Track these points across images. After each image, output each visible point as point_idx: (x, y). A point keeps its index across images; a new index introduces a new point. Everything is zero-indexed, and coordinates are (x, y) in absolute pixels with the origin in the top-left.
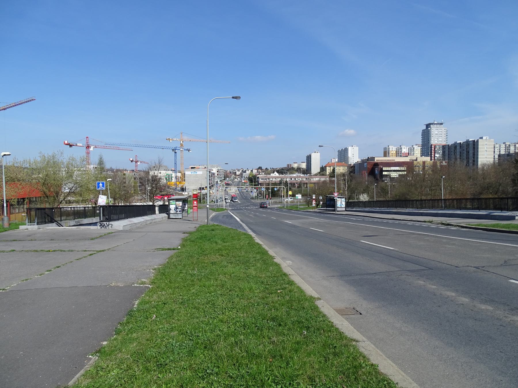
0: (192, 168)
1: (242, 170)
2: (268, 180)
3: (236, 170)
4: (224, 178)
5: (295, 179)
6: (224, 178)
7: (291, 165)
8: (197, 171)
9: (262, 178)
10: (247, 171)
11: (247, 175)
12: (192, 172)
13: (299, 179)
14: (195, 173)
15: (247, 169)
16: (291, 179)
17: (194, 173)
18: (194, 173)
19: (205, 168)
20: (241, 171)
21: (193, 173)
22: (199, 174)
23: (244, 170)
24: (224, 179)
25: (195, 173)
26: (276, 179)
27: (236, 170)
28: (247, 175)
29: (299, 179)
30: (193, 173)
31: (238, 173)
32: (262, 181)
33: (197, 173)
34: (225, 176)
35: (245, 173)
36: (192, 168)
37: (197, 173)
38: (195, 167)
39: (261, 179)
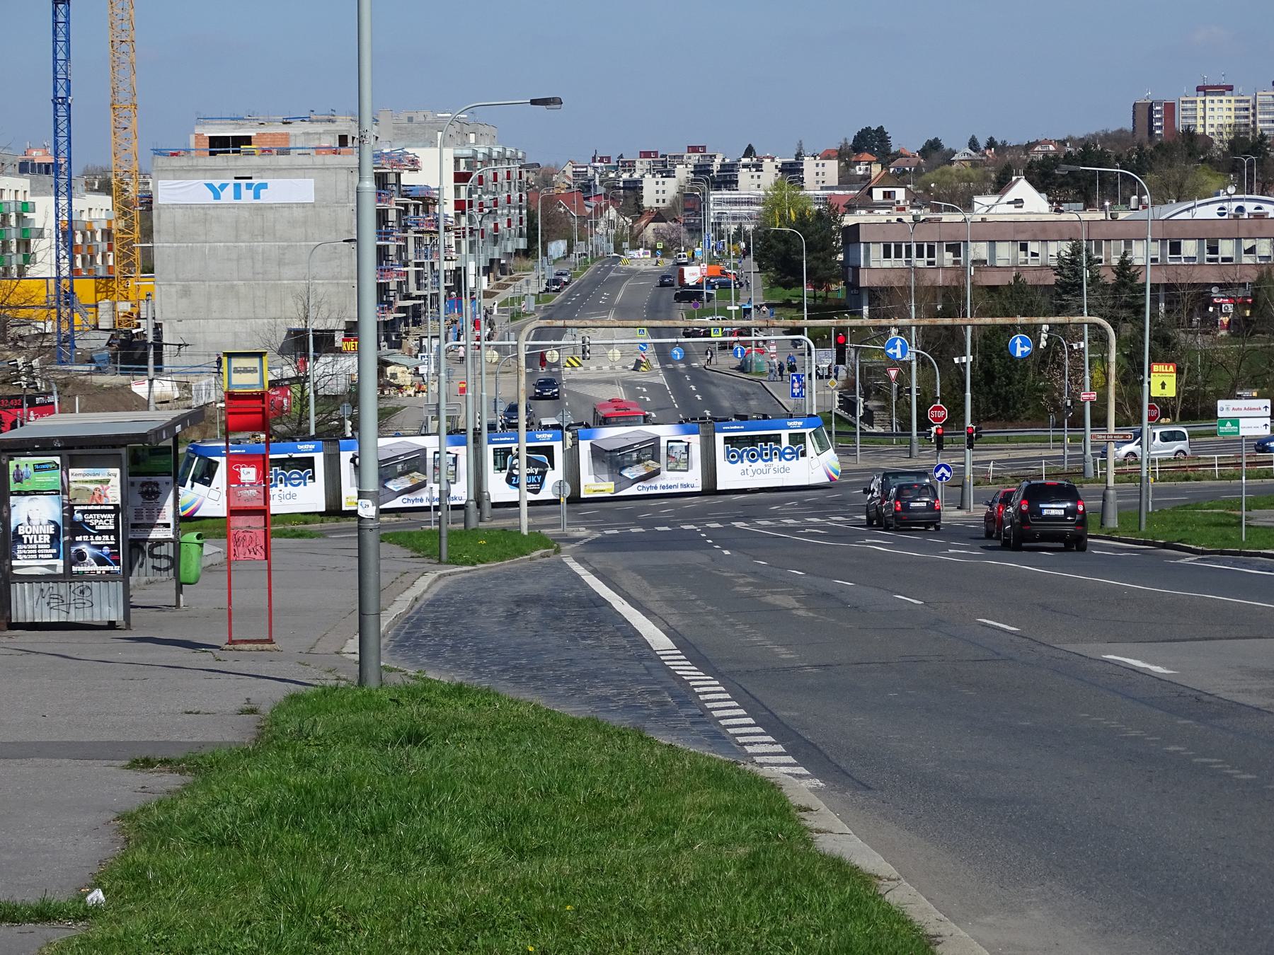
0: (219, 145)
1: (695, 158)
2: (949, 256)
3: (641, 165)
4: (522, 244)
5: (1214, 250)
6: (522, 244)
7: (1170, 108)
8: (262, 170)
9: (893, 238)
10: (744, 176)
11: (744, 210)
12: (217, 183)
13: (1247, 244)
14: (248, 196)
15: (749, 152)
16: (1176, 248)
17: (237, 195)
18: (237, 195)
19: (343, 140)
20: (683, 172)
21: (227, 196)
22: (289, 206)
23: (716, 167)
24: (528, 253)
25: (248, 196)
26: (1024, 247)
27: (641, 165)
28: (744, 210)
29: (1251, 250)
30: (227, 196)
31: (656, 192)
32: (887, 264)
33: (266, 197)
34: (531, 217)
35: (725, 194)
36: (219, 145)
37: (266, 197)
38: (247, 140)
39: (877, 251)
